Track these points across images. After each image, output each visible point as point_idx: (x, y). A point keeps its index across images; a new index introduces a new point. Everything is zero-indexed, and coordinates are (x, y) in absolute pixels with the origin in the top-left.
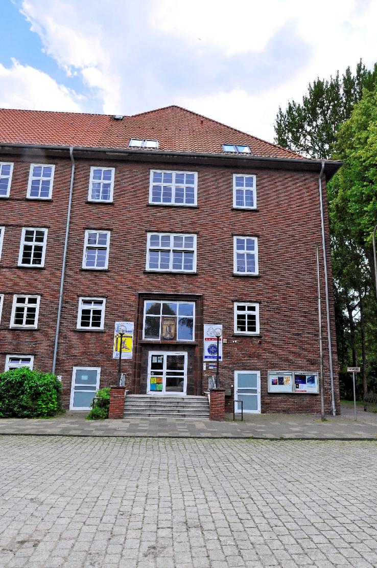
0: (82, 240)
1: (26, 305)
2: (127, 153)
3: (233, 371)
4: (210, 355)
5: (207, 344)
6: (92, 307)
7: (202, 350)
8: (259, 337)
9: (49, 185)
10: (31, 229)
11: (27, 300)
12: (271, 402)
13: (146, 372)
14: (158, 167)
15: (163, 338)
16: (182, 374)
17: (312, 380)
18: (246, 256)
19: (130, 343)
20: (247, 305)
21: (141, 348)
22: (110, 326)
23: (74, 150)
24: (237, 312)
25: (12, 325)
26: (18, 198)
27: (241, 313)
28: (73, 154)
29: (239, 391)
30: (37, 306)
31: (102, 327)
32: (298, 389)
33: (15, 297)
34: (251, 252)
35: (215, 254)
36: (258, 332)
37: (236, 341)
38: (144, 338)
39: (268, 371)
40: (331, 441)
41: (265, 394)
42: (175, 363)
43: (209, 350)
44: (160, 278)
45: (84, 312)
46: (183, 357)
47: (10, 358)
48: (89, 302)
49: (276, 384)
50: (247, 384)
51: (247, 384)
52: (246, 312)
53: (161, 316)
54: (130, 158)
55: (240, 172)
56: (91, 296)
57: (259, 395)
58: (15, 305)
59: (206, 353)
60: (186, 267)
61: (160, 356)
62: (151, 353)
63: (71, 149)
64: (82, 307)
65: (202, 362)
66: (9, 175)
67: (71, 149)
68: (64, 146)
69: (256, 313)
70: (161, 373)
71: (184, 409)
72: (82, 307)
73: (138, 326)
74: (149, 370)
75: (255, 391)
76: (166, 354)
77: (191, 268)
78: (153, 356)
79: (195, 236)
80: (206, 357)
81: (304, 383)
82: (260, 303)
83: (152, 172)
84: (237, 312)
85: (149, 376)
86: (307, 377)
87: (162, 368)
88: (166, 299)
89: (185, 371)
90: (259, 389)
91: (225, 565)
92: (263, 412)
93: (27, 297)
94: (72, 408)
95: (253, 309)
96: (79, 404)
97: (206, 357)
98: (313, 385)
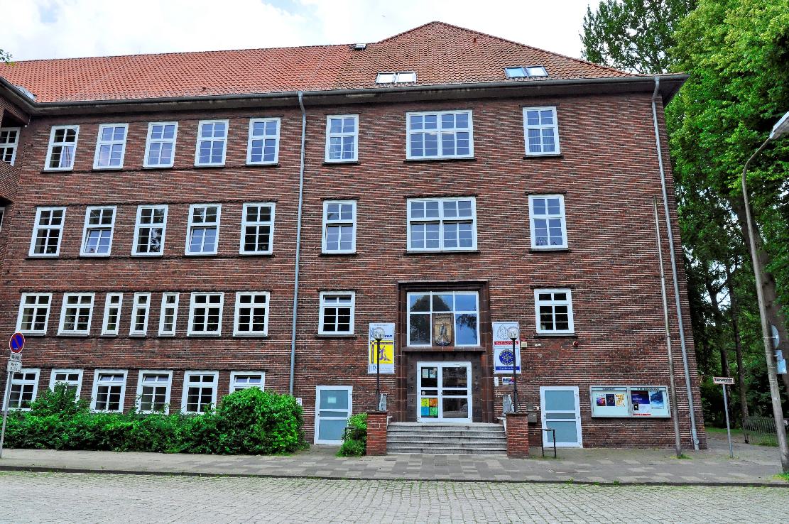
5: (497, 351)
11: (208, 299)
15: (436, 344)
17: (659, 398)
18: (549, 221)
19: (389, 351)
21: (406, 358)
22: (362, 330)
24: (539, 304)
25: (61, 331)
28: (303, 100)
31: (351, 332)
35: (504, 225)
42: (454, 378)
46: (464, 370)
49: (603, 404)
50: (558, 404)
53: (431, 312)
54: (379, 100)
56: (331, 287)
59: (497, 362)
61: (432, 368)
62: (420, 365)
63: (300, 95)
67: (300, 95)
70: (435, 393)
72: (323, 304)
73: (401, 329)
74: (419, 388)
75: (573, 416)
76: (440, 366)
77: (470, 245)
78: (422, 368)
80: (498, 368)
81: (647, 402)
84: (539, 304)
85: (419, 397)
86: (650, 394)
88: (458, 288)
89: (469, 389)
90: (577, 412)
92: (585, 445)
97: (498, 368)
98: (660, 405)
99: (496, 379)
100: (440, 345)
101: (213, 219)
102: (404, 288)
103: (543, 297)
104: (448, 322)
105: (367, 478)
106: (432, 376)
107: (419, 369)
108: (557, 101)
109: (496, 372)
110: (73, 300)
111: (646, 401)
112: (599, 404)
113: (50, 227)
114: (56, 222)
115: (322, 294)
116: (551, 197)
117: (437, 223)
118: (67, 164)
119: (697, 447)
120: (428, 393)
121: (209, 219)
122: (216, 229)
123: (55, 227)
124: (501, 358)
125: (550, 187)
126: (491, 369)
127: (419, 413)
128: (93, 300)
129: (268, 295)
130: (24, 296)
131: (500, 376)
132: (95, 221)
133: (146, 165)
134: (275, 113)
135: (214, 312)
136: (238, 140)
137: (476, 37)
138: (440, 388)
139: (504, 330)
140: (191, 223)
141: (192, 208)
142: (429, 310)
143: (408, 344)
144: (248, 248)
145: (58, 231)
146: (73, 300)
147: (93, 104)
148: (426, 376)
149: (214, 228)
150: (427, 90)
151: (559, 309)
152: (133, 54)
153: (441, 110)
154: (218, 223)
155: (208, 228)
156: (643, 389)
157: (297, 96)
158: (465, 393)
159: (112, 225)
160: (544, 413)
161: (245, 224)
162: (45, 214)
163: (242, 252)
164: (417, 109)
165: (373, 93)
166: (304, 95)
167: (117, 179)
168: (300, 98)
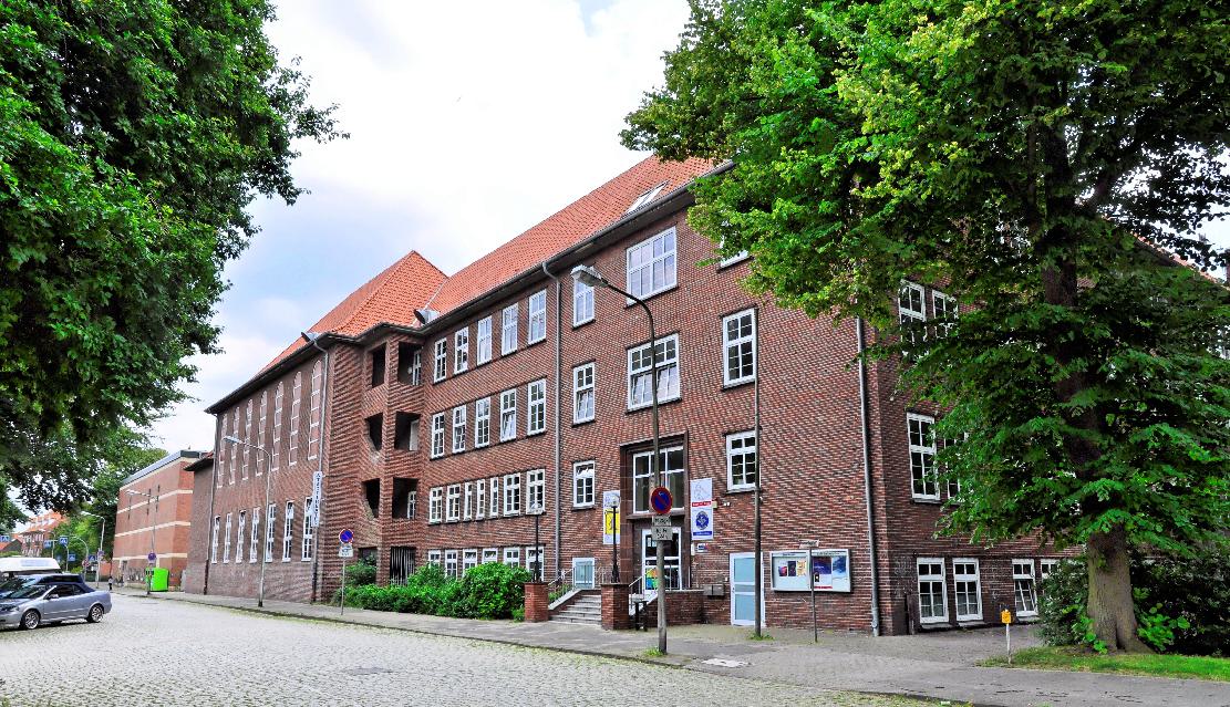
28: (548, 270)
45: (737, 459)
56: (583, 462)
59: (695, 528)
68: (534, 265)
72: (577, 476)
74: (644, 559)
80: (695, 534)
85: (644, 567)
86: (833, 560)
94: (733, 621)
97: (695, 534)
98: (842, 575)
102: (627, 451)
105: (1181, 673)
109: (694, 538)
111: (827, 570)
112: (781, 575)
113: (740, 341)
114: (747, 332)
118: (484, 356)
119: (876, 632)
123: (746, 339)
124: (698, 524)
130: (730, 439)
131: (697, 542)
136: (610, 287)
141: (502, 395)
144: (734, 374)
145: (749, 344)
147: (495, 291)
152: (587, 193)
157: (541, 268)
166: (548, 264)
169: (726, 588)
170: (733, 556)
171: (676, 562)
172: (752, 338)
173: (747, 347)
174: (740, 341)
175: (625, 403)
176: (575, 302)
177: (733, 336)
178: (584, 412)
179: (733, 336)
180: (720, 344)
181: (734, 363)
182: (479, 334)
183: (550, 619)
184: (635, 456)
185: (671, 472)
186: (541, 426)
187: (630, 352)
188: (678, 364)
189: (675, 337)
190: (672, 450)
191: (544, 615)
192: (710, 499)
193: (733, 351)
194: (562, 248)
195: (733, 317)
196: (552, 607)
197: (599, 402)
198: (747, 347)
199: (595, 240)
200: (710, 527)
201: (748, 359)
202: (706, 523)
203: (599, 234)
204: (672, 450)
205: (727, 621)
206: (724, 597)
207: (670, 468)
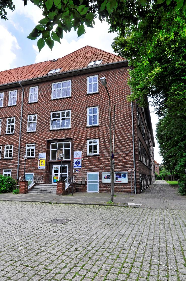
0: (86, 112)
1: (9, 150)
2: (40, 79)
3: (86, 173)
4: (77, 166)
5: (75, 161)
6: (31, 148)
7: (73, 163)
8: (99, 156)
9: (70, 90)
10: (54, 113)
11: (9, 148)
12: (104, 187)
13: (52, 174)
14: (55, 82)
15: (58, 159)
16: (66, 175)
17: (124, 176)
18: (93, 116)
19: (44, 162)
20: (93, 141)
21: (49, 164)
22: (37, 155)
23: (21, 82)
24: (88, 145)
25: (5, 158)
26: (6, 106)
27: (90, 145)
28: (21, 84)
29: (89, 182)
30: (12, 149)
31: (34, 156)
32: (117, 181)
33: (5, 146)
34: (90, 115)
35: (80, 118)
36: (98, 154)
37: (87, 159)
38: (51, 160)
39: (102, 172)
40: (72, 205)
41: (101, 184)
42: (63, 170)
43: (76, 163)
44: (56, 132)
45: (90, 147)
46: (66, 167)
47: (5, 171)
48: (91, 142)
49: (106, 178)
50: (93, 179)
51: (93, 179)
52: (93, 144)
53: (64, 149)
54: (43, 80)
55: (64, 80)
56: (30, 143)
57: (98, 184)
58: (5, 149)
59: (75, 165)
60: (62, 126)
61: (57, 167)
62: (54, 166)
63: (20, 82)
64: (27, 148)
65: (73, 169)
66: (70, 86)
67: (20, 82)
68: (17, 81)
69: (98, 144)
70: (57, 175)
71: (47, 190)
72: (27, 148)
73: (48, 155)
74: (53, 173)
75: (97, 182)
76: (59, 166)
77: (97, 124)
78: (54, 167)
79: (98, 108)
80: (75, 167)
81: (121, 177)
82: (99, 139)
83: (88, 78)
84: (88, 145)
85: (53, 176)
86: (122, 175)
87: (58, 173)
88: (67, 141)
89: (67, 173)
90: (98, 181)
91: (166, 279)
92: (100, 192)
93: (9, 146)
94: (88, 191)
95: (33, 146)
96: (93, 189)
97: (75, 167)
98: (125, 178)
99: (74, 170)
100: (59, 160)
101: (68, 115)
102: (49, 142)
103: (90, 143)
104: (61, 152)
106: (57, 170)
107: (53, 167)
108: (98, 73)
109: (74, 168)
110: (7, 148)
111: (120, 177)
112: (105, 178)
113: (11, 124)
115: (27, 145)
116: (94, 107)
117: (59, 120)
119: (135, 193)
120: (56, 175)
121: (58, 117)
122: (60, 120)
125: (94, 105)
126: (73, 167)
127: (53, 181)
128: (35, 146)
129: (13, 146)
130: (88, 141)
132: (54, 117)
133: (9, 105)
134: (15, 89)
135: (11, 151)
136: (45, 95)
137: (5, 71)
138: (59, 173)
139: (78, 154)
140: (52, 119)
141: (8, 119)
142: (64, 148)
143: (50, 160)
146: (7, 148)
147: (7, 85)
148: (55, 169)
149: (69, 119)
150: (56, 75)
151: (94, 146)
153: (62, 81)
154: (70, 117)
155: (57, 120)
156: (119, 173)
158: (17, 173)
159: (36, 121)
160: (88, 181)
161: (8, 124)
162: (54, 114)
163: (7, 133)
164: (62, 80)
165: (40, 79)
167: (36, 105)
168: (20, 83)
169: (86, 182)
170: (88, 173)
171: (66, 175)
172: (14, 124)
173: (13, 126)
174: (11, 124)
175: (86, 124)
176: (9, 99)
177: (9, 123)
178: (31, 128)
179: (9, 123)
180: (86, 115)
181: (9, 129)
182: (9, 96)
183: (28, 193)
184: (51, 144)
185: (64, 148)
186: (12, 131)
187: (52, 113)
188: (36, 122)
189: (70, 111)
190: (66, 142)
191: (27, 191)
192: (81, 157)
193: (9, 126)
194: (28, 79)
195: (64, 111)
196: (29, 188)
197: (38, 125)
198: (13, 126)
199: (42, 79)
200: (80, 165)
201: (12, 129)
202: (79, 163)
203: (75, 70)
204: (66, 142)
205: (86, 191)
206: (85, 185)
207: (64, 148)
